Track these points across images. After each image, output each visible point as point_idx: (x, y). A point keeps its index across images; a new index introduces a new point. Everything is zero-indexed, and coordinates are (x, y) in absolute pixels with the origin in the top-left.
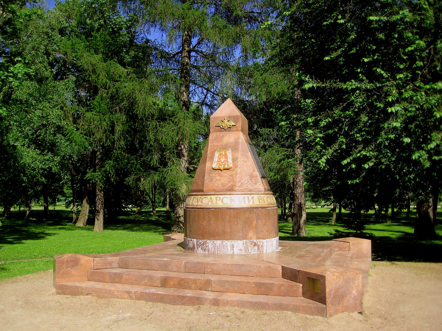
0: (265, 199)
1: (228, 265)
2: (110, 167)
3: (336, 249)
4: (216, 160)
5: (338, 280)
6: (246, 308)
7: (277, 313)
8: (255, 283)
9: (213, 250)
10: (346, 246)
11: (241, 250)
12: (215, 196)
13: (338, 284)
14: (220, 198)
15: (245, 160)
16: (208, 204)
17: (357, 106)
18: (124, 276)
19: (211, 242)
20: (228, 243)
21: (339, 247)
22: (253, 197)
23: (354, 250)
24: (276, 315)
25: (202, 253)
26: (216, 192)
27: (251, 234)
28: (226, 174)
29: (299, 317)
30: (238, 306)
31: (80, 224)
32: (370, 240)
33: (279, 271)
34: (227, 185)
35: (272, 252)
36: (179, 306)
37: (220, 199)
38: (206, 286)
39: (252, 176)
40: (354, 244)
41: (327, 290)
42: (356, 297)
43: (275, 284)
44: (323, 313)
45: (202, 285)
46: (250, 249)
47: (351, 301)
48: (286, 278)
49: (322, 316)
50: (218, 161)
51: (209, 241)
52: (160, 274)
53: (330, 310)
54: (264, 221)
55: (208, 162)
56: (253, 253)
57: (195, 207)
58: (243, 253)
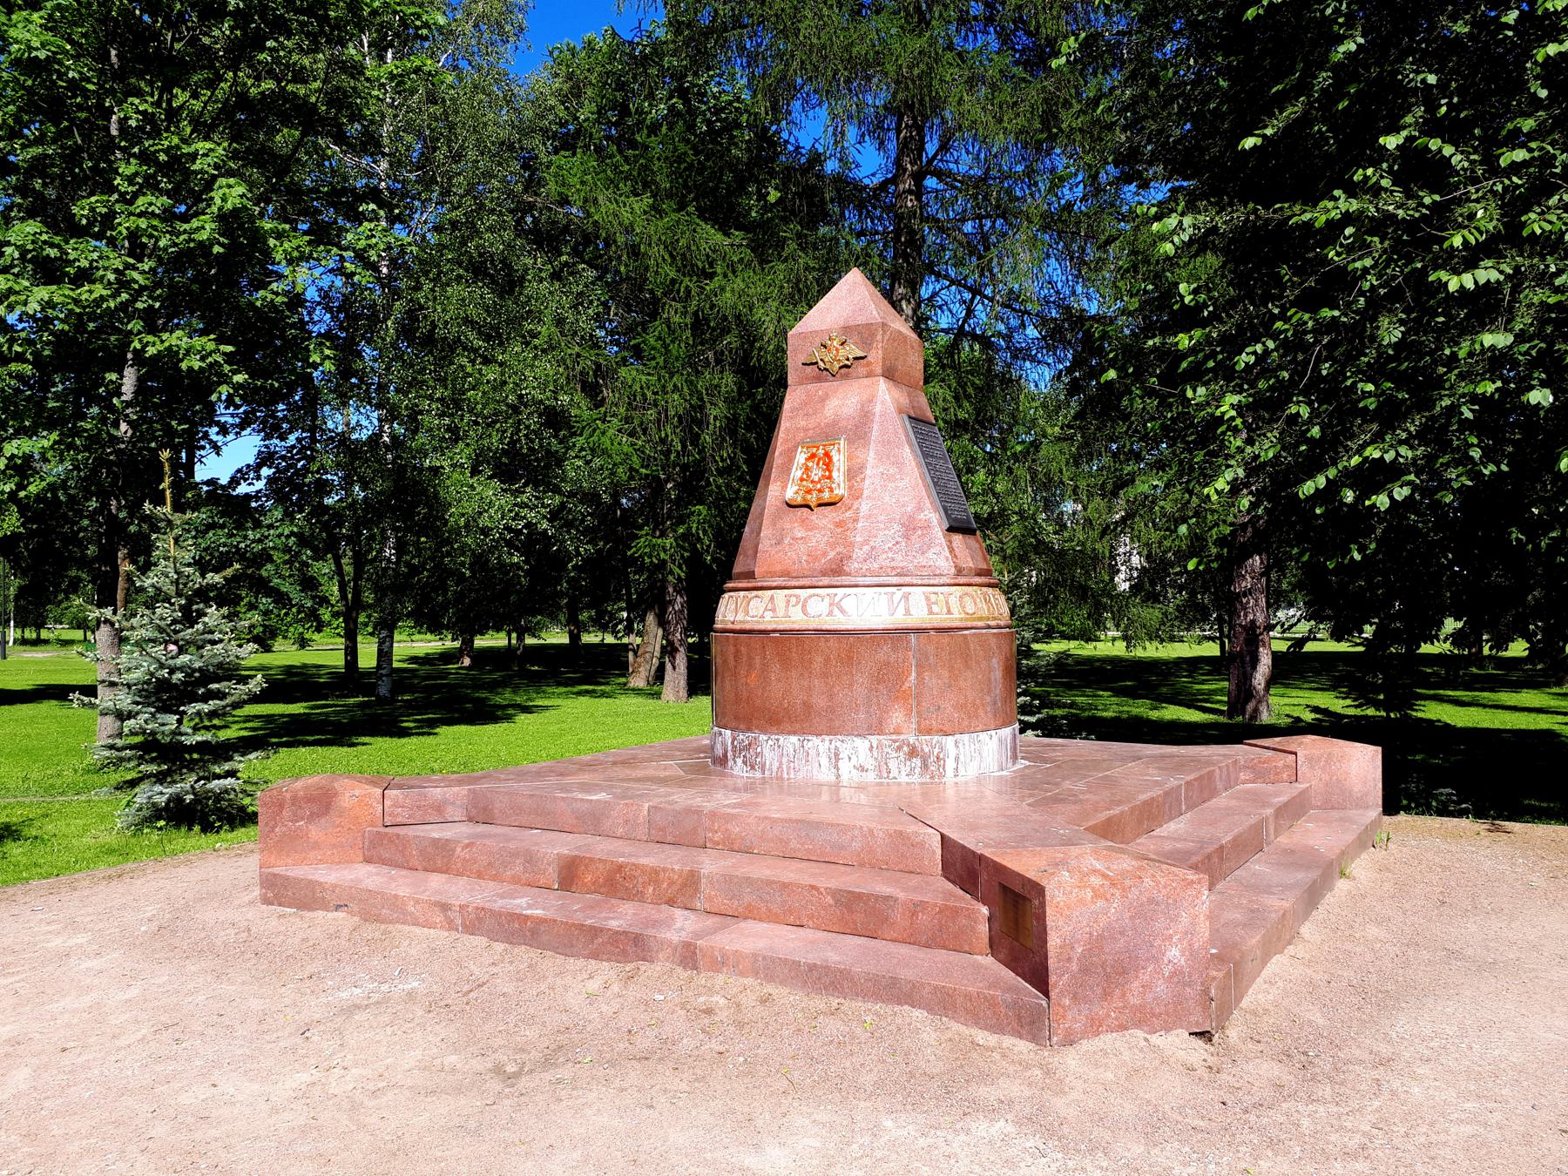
0: (953, 601)
1: (774, 821)
2: (699, 522)
3: (1242, 776)
4: (799, 474)
5: (1100, 903)
6: (781, 983)
7: (877, 1014)
8: (834, 893)
9: (776, 764)
10: (1281, 764)
11: (862, 769)
12: (786, 592)
13: (1103, 921)
14: (797, 597)
15: (891, 471)
16: (762, 617)
17: (1366, 286)
18: (459, 849)
19: (770, 742)
20: (819, 745)
21: (1253, 768)
22: (906, 597)
23: (1312, 779)
24: (869, 1019)
25: (745, 775)
26: (792, 580)
27: (897, 717)
28: (824, 518)
29: (949, 1035)
30: (756, 974)
31: (638, 681)
32: (1380, 749)
33: (934, 852)
34: (825, 554)
35: (979, 780)
36: (581, 962)
37: (798, 603)
38: (684, 891)
39: (910, 527)
40: (1310, 759)
41: (1053, 941)
42: (1182, 972)
43: (896, 899)
44: (1032, 1026)
45: (675, 888)
46: (893, 764)
47: (1161, 988)
48: (952, 878)
49: (1034, 1039)
50: (802, 480)
51: (765, 738)
52: (558, 846)
53: (1064, 1017)
54: (945, 673)
55: (775, 481)
56: (903, 779)
57: (730, 626)
58: (871, 777)
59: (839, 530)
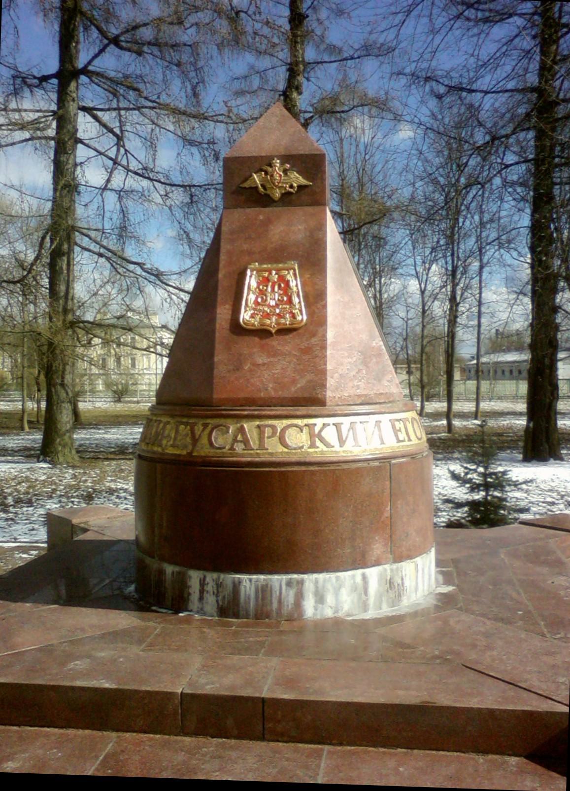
28: (285, 345)
59: (306, 357)
